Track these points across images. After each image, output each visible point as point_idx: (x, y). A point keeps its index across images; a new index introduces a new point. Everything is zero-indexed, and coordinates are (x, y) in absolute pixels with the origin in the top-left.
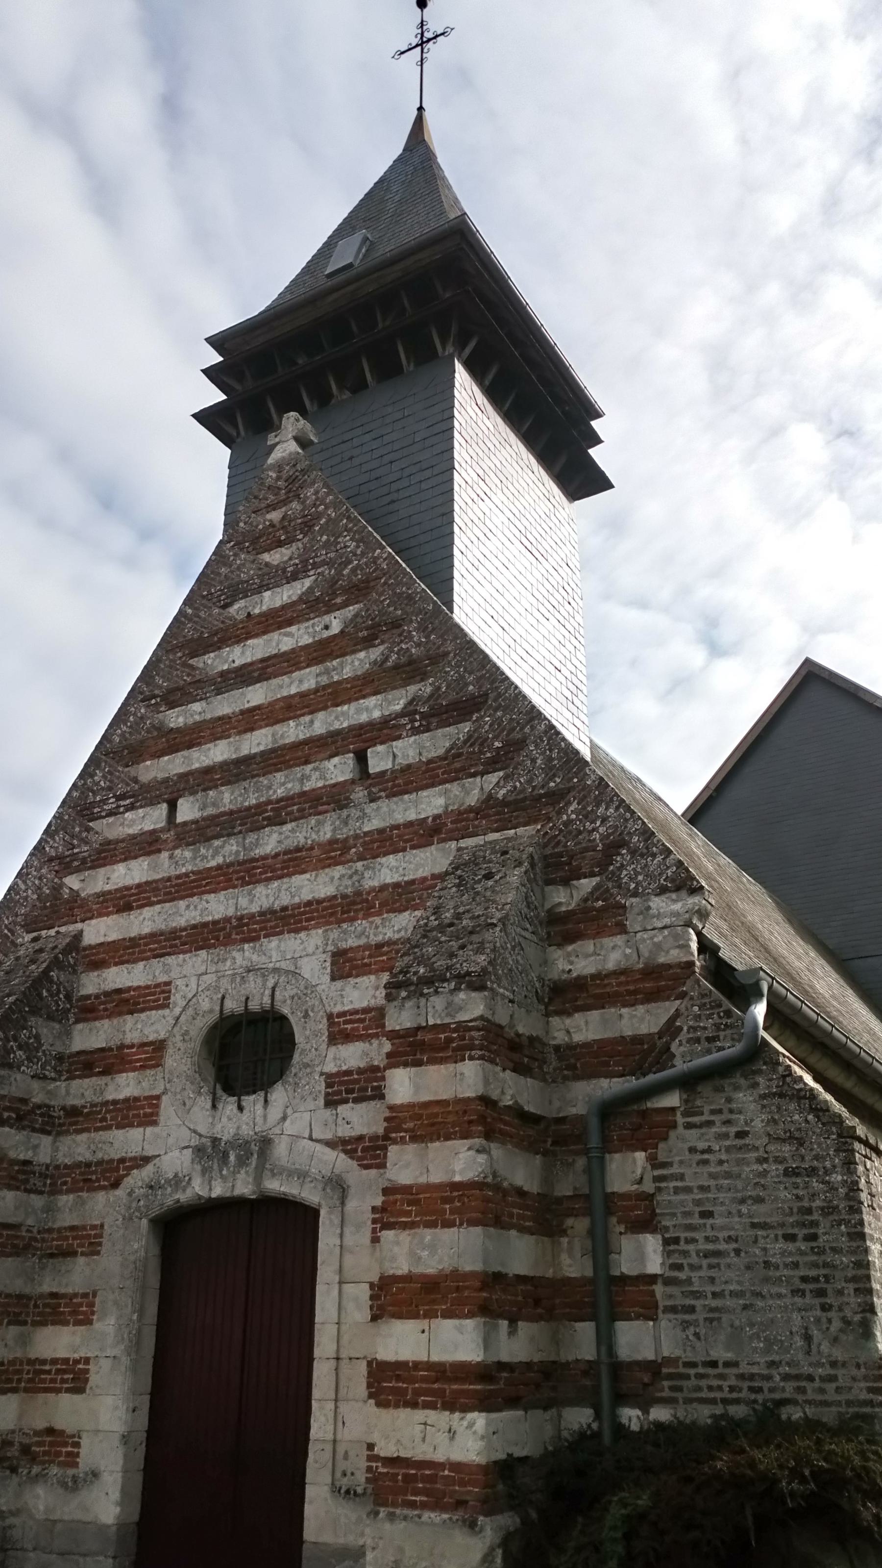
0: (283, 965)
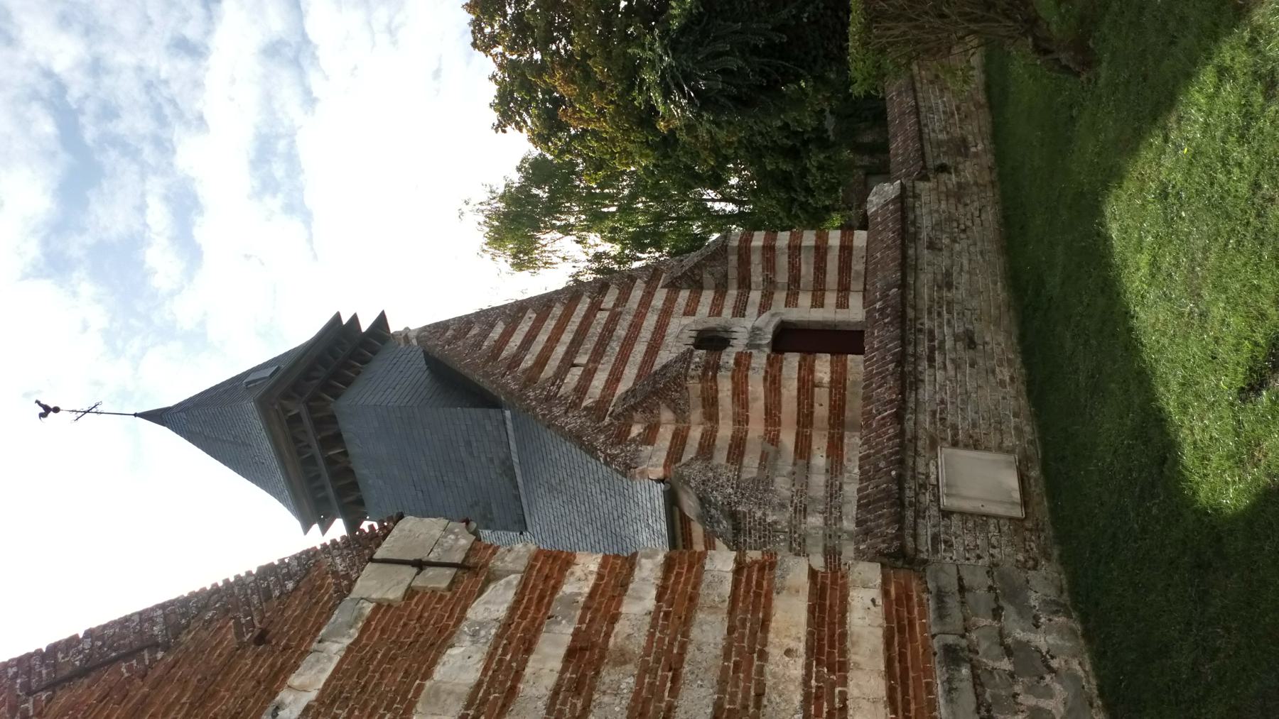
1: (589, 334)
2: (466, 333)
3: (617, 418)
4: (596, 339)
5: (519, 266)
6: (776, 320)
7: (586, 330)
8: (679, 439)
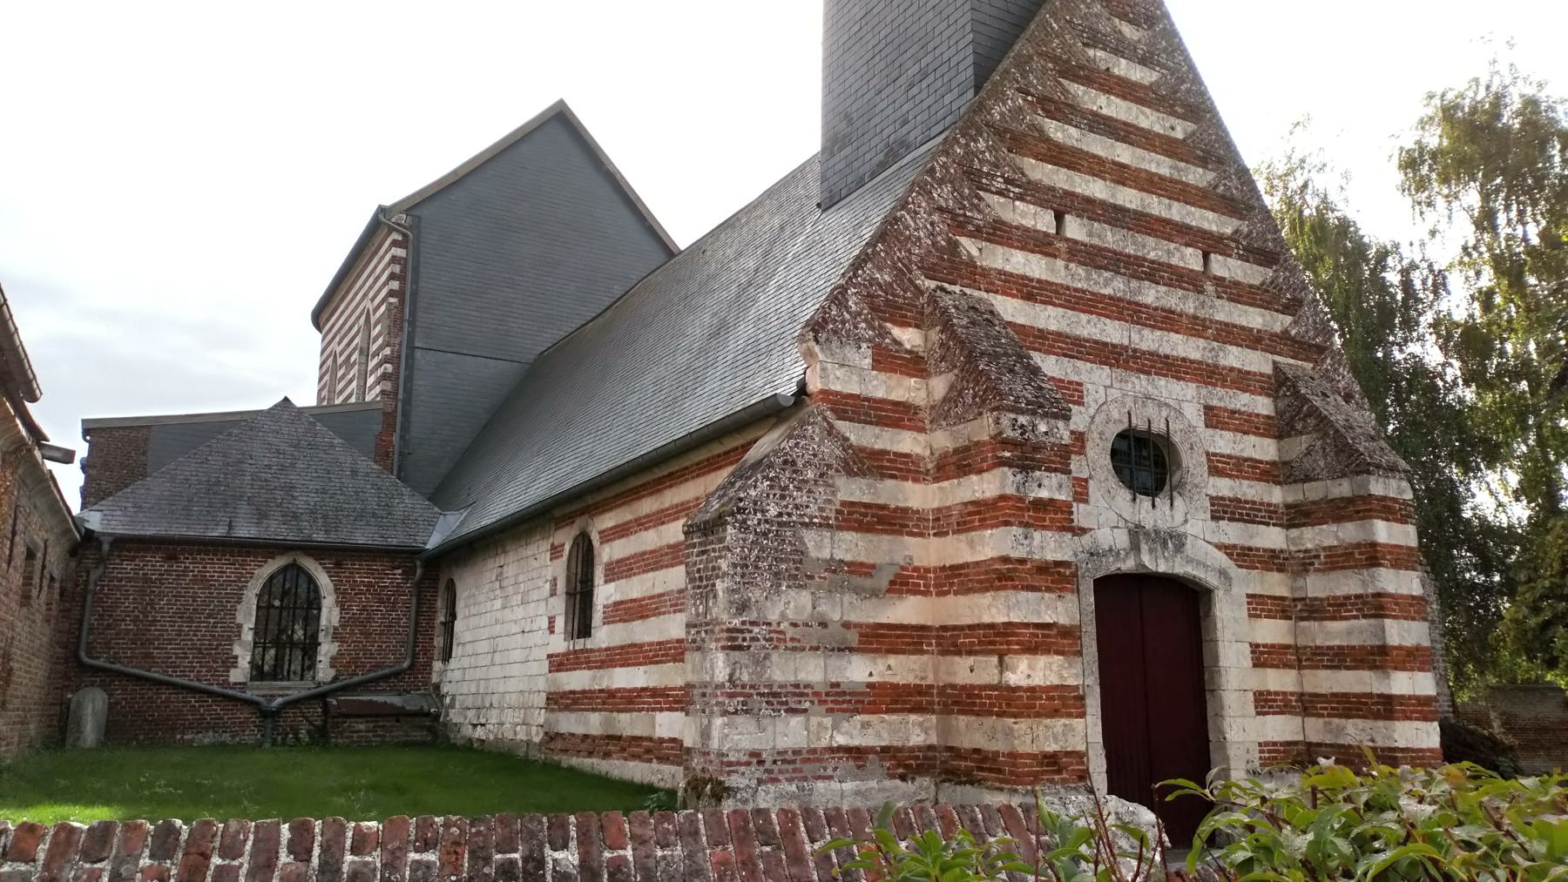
0: (1171, 403)
1: (1140, 238)
2: (1124, 17)
3: (933, 300)
4: (1130, 250)
5: (1410, 163)
6: (1211, 579)
7: (1151, 232)
8: (897, 415)
